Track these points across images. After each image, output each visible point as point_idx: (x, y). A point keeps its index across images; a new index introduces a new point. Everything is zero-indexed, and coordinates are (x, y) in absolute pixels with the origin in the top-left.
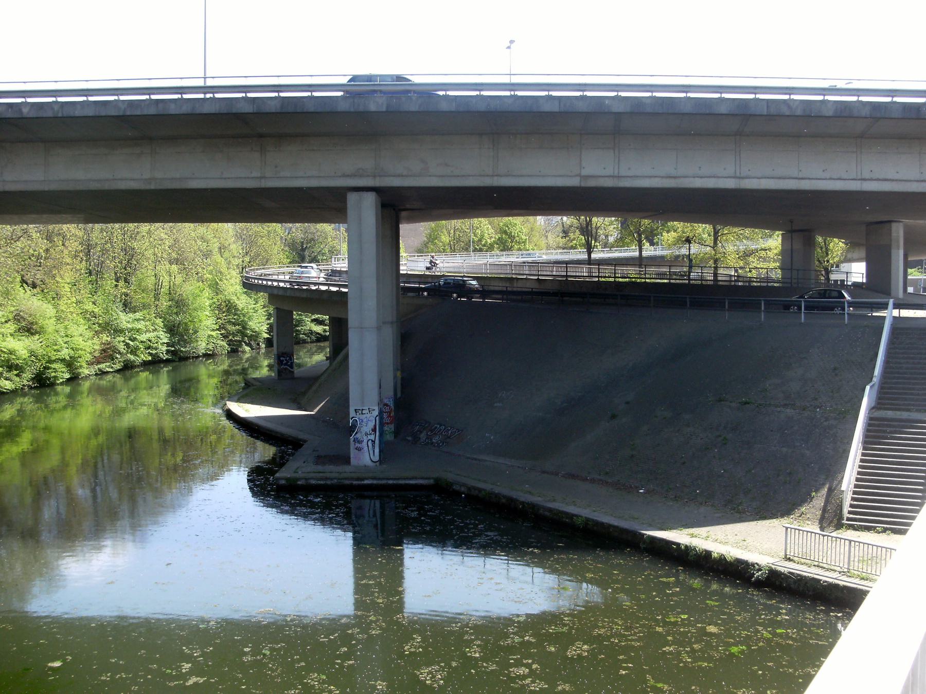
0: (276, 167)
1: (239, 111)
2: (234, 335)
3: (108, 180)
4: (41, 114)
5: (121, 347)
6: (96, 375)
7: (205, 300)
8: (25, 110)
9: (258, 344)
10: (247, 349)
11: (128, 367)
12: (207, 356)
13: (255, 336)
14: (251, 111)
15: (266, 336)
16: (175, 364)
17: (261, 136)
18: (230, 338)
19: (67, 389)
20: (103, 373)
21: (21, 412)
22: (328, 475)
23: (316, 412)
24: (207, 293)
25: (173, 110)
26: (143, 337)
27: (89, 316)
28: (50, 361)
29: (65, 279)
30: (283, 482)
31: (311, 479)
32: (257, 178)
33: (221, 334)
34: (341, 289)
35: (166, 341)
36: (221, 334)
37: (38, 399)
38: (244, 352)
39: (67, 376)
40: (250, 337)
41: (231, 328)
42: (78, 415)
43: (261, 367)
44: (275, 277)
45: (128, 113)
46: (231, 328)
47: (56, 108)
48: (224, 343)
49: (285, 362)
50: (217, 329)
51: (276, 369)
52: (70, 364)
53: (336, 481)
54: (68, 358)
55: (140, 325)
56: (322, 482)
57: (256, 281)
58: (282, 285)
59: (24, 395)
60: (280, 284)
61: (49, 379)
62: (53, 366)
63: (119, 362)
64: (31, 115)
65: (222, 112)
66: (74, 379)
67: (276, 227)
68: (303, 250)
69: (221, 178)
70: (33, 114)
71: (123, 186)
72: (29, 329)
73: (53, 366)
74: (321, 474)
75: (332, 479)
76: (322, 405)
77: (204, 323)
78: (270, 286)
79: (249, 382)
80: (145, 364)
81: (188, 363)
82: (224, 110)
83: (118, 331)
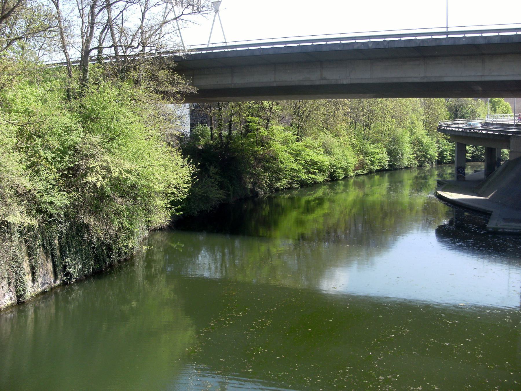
0: (490, 70)
1: (479, 43)
2: (421, 157)
3: (402, 78)
4: (378, 47)
5: (368, 162)
6: (356, 176)
7: (407, 138)
8: (370, 45)
9: (432, 163)
10: (427, 165)
11: (370, 172)
12: (407, 168)
13: (431, 159)
14: (484, 43)
15: (437, 158)
16: (391, 172)
17: (483, 54)
18: (419, 159)
19: (343, 182)
20: (359, 175)
21: (324, 194)
22: (515, 227)
23: (489, 198)
24: (408, 134)
25: (444, 43)
26: (378, 156)
27: (354, 146)
28: (337, 168)
29: (342, 126)
30: (491, 230)
31: (506, 229)
32: (480, 76)
33: (414, 157)
34: (482, 131)
35: (388, 159)
36: (414, 157)
37: (332, 188)
38: (426, 167)
39: (343, 176)
40: (429, 159)
41: (420, 154)
42: (348, 195)
43: (434, 175)
44: (453, 126)
45: (421, 45)
46: (420, 154)
47: (385, 44)
48: (416, 162)
49: (461, 172)
50: (412, 154)
51: (456, 176)
52: (345, 170)
53: (518, 230)
54: (344, 167)
55: (377, 150)
56: (511, 231)
57: (444, 128)
58: (460, 130)
59: (324, 185)
60: (459, 129)
61: (336, 177)
62: (338, 170)
63: (367, 170)
64: (373, 48)
65: (469, 44)
66: (346, 178)
67: (443, 100)
68: (457, 111)
69: (461, 76)
70: (374, 47)
71: (410, 80)
72: (328, 152)
73: (338, 170)
74: (511, 227)
75: (516, 229)
76: (492, 194)
77: (407, 150)
78: (457, 131)
79: (440, 182)
80: (378, 171)
81: (396, 171)
82: (470, 43)
83: (366, 154)
